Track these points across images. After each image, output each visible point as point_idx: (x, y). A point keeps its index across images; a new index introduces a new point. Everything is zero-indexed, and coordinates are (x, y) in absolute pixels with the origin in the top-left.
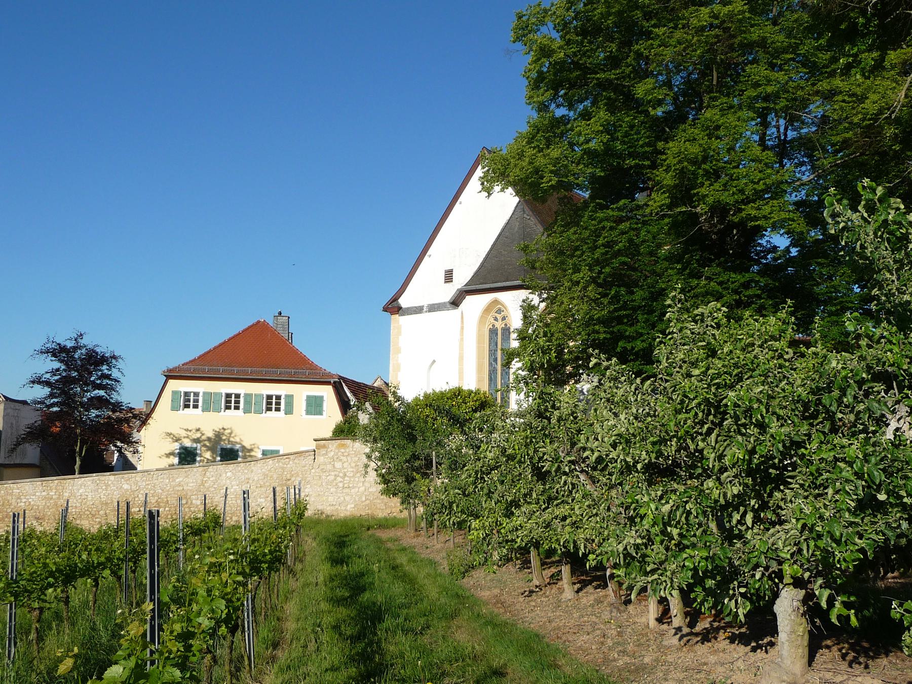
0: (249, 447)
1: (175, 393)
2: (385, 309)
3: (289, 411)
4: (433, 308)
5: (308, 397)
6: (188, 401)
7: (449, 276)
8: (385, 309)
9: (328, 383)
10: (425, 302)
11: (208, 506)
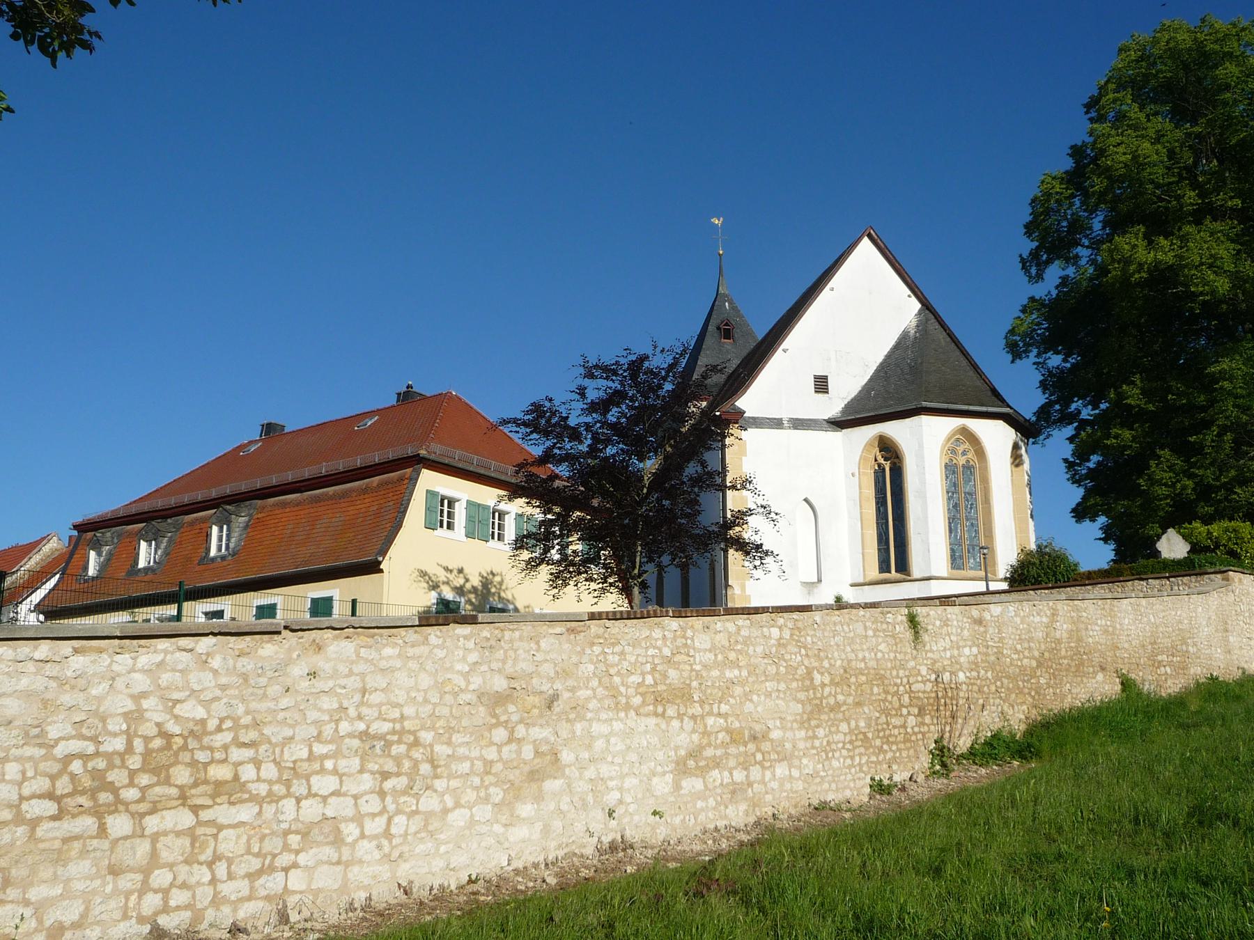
4: (798, 424)
7: (821, 385)
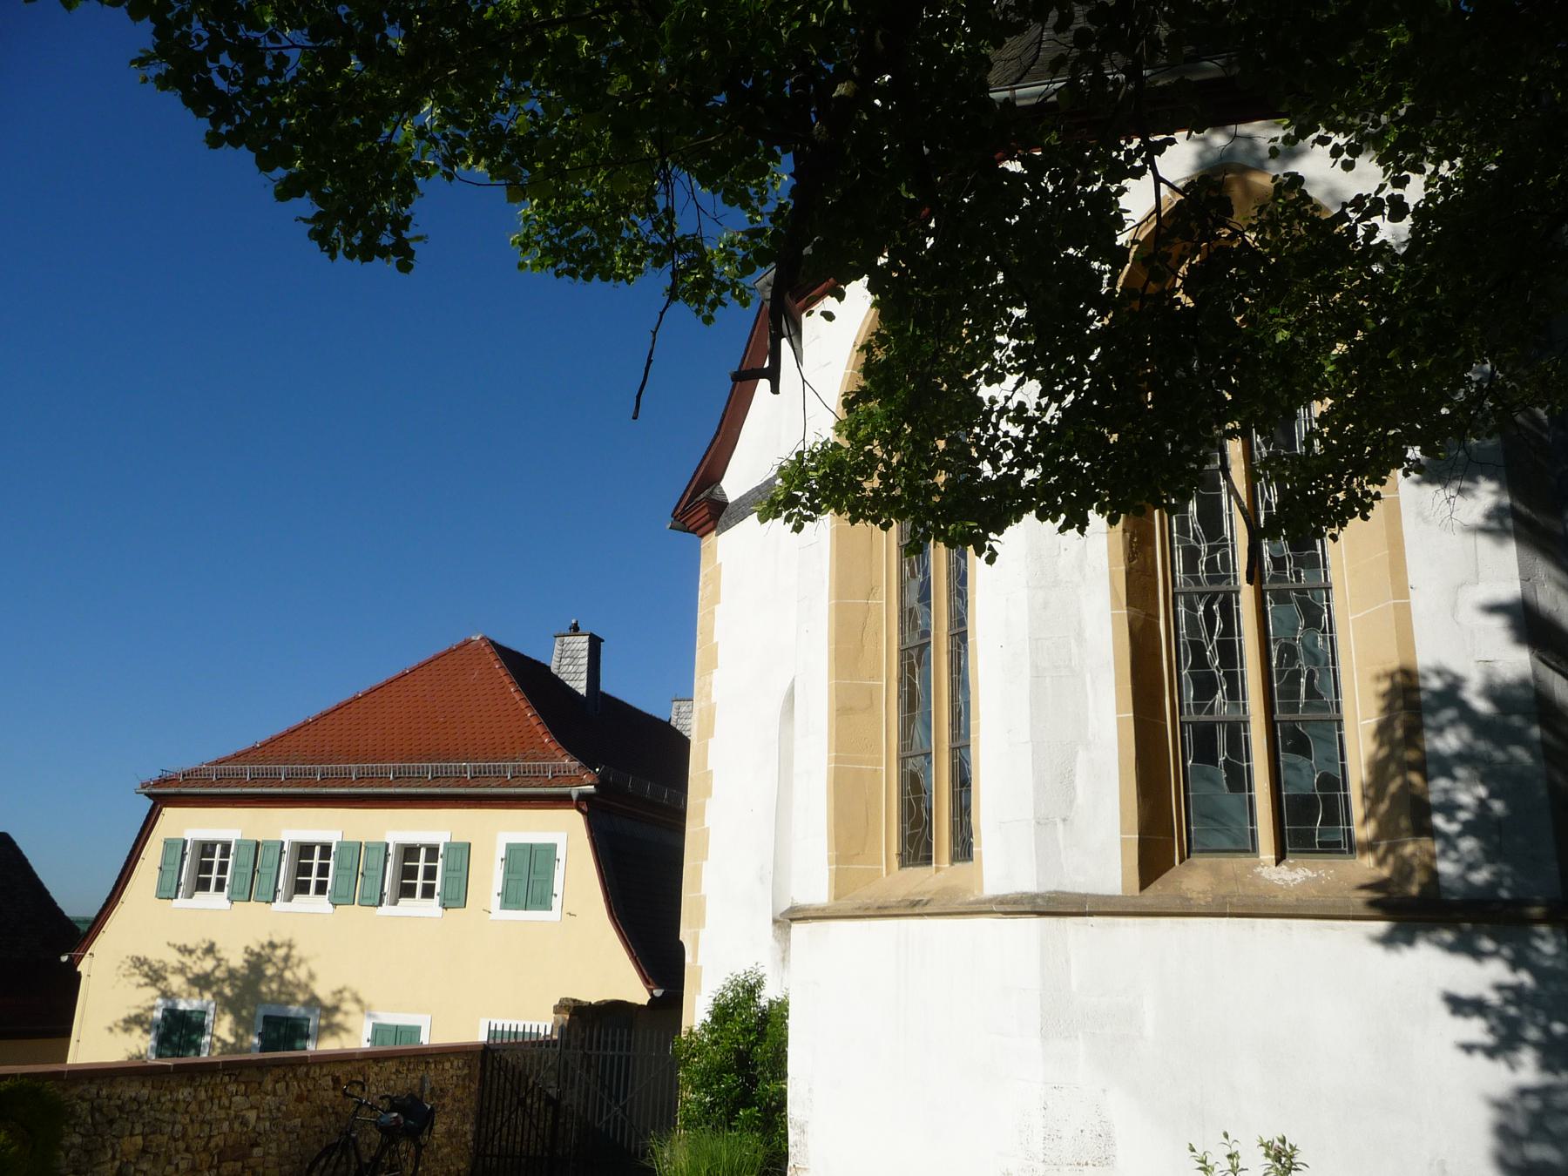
0: (328, 1000)
1: (169, 844)
3: (456, 899)
5: (512, 849)
6: (204, 868)
9: (560, 801)
11: (1178, 185)
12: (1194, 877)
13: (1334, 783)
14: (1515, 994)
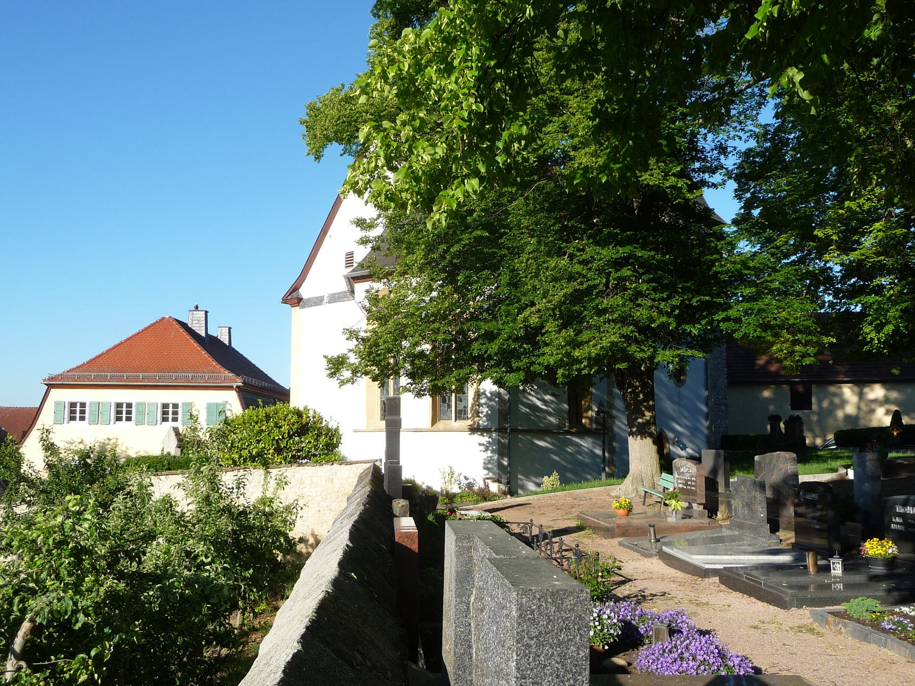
1: (57, 404)
2: (285, 301)
6: (76, 412)
8: (285, 301)
9: (231, 388)
10: (326, 292)
12: (440, 424)
13: (465, 407)
14: (489, 443)
